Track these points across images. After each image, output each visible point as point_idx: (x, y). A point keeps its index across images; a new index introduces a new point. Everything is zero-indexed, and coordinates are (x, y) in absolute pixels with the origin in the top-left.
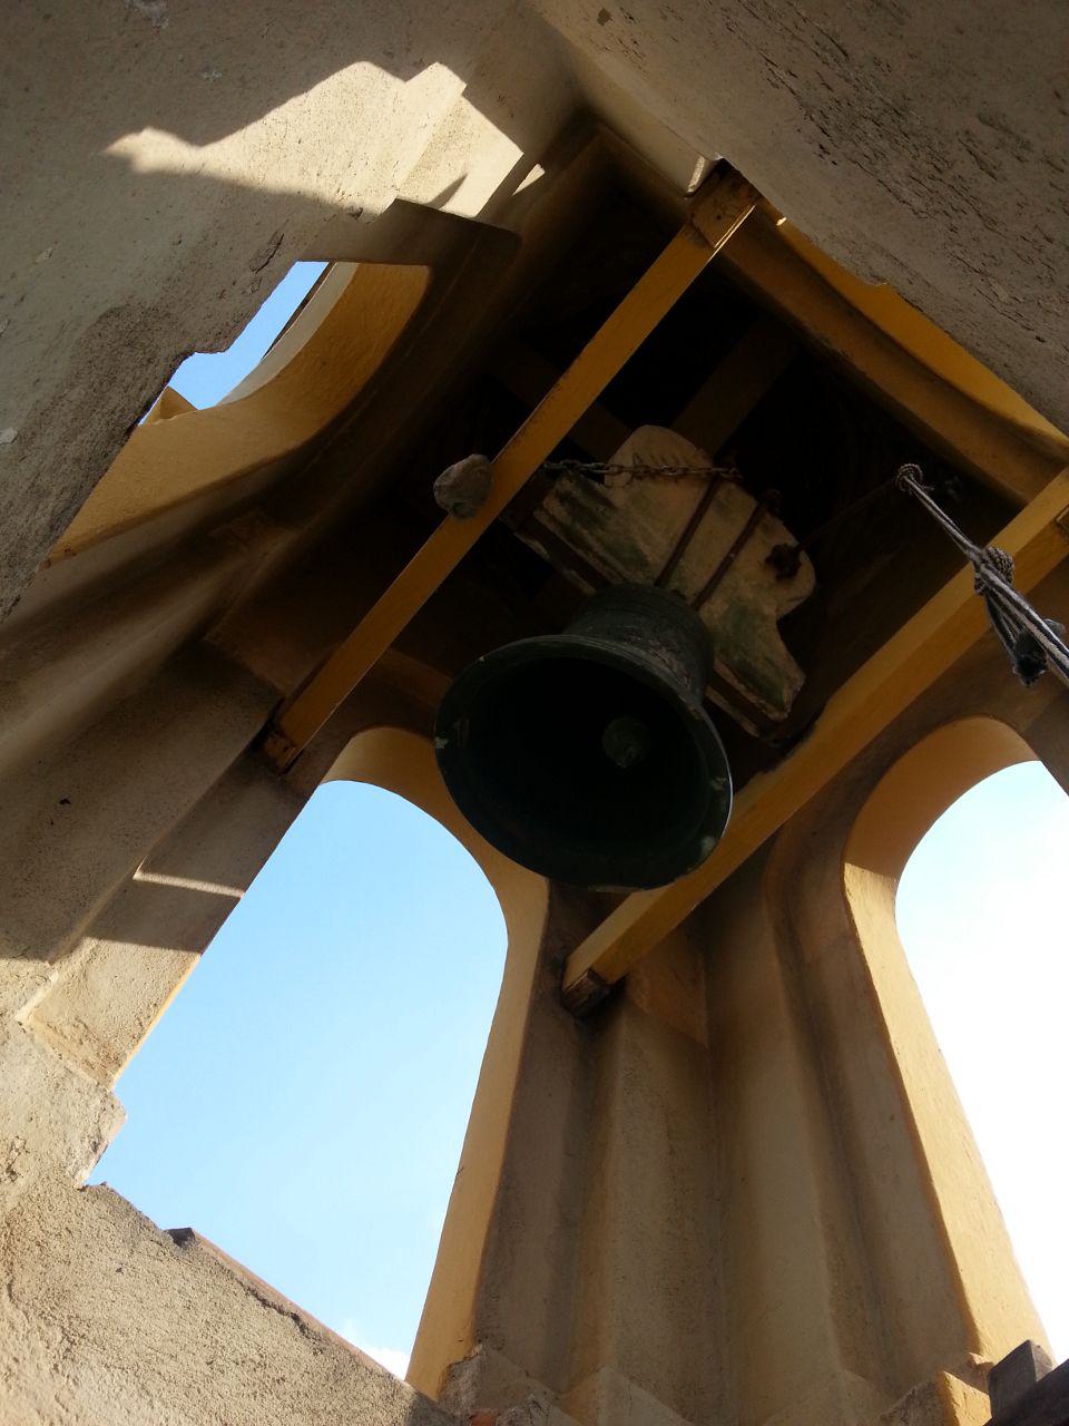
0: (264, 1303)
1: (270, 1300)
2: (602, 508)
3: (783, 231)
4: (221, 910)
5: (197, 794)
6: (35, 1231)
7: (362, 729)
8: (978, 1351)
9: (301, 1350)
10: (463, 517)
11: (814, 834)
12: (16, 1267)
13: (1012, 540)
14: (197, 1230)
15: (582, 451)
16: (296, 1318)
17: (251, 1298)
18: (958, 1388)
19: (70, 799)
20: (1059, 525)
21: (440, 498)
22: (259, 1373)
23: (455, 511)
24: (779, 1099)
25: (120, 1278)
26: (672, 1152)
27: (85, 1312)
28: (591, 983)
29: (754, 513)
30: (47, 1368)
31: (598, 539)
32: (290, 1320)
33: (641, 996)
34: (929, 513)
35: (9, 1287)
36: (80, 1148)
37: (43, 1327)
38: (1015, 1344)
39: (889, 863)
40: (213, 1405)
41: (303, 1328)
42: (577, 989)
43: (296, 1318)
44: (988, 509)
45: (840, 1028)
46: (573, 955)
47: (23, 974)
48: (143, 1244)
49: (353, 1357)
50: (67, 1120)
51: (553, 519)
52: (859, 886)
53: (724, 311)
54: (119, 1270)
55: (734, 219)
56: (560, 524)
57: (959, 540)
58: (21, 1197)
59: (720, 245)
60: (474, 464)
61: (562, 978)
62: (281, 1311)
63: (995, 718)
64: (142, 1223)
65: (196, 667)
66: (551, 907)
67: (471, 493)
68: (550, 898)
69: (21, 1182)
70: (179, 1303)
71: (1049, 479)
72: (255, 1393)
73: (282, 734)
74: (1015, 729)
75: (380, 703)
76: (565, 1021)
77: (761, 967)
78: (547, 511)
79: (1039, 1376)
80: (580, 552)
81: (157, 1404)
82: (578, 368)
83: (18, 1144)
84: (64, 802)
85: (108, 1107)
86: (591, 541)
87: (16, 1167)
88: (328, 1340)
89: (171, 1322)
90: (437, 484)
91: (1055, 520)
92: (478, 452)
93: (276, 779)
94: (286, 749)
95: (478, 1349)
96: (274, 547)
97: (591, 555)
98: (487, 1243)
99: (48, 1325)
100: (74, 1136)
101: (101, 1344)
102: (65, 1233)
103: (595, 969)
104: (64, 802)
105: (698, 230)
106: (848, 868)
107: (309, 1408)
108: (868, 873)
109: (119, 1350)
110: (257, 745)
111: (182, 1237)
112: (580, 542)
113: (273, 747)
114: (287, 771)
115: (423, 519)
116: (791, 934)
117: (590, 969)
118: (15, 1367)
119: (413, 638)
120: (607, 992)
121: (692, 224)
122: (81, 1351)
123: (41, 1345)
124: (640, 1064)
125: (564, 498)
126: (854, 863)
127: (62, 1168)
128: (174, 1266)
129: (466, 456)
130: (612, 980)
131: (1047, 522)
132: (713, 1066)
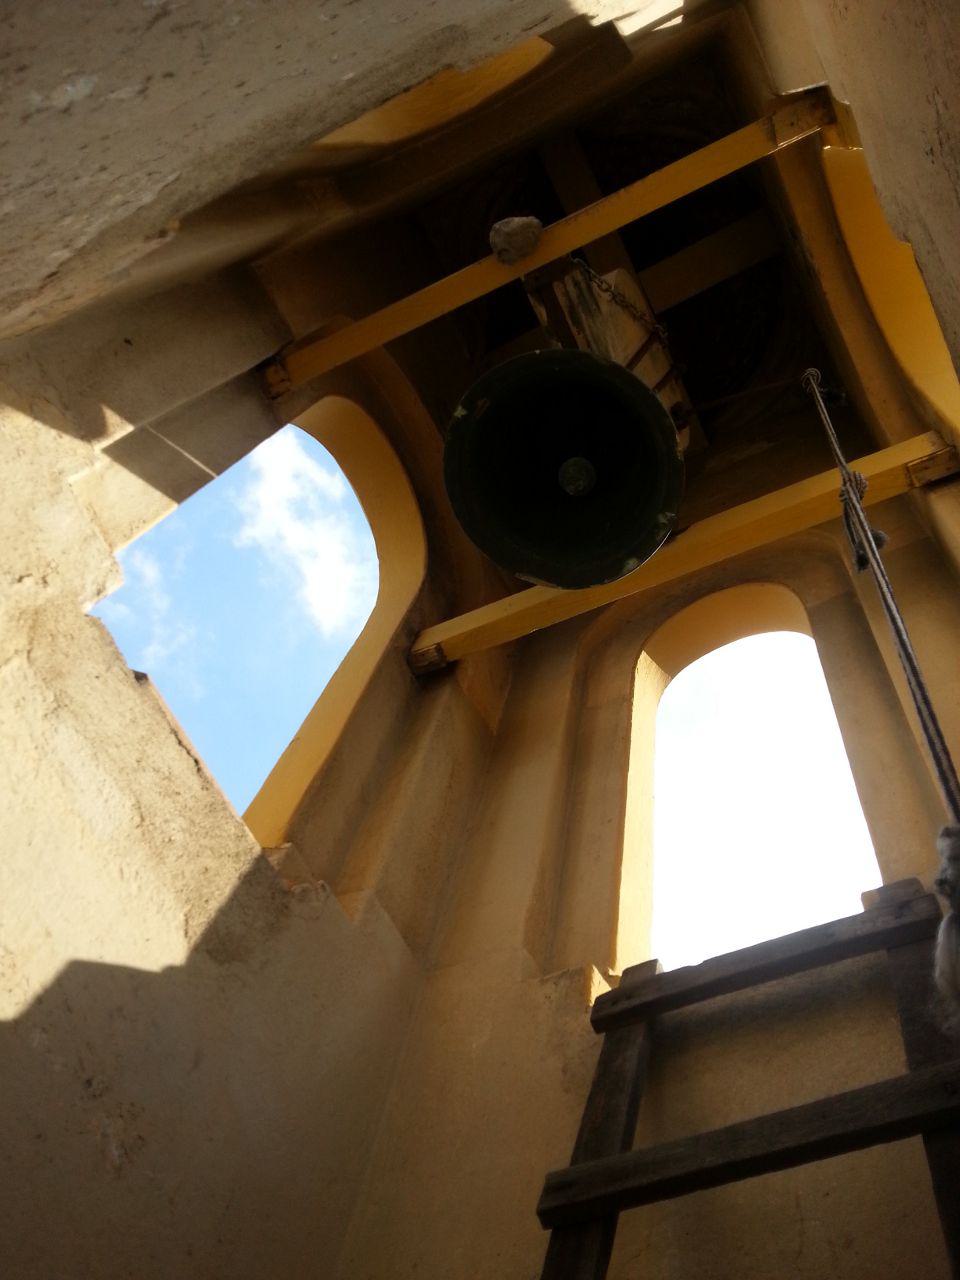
0: (180, 743)
1: (185, 742)
2: (594, 307)
3: (825, 155)
4: (202, 480)
5: (220, 381)
6: (51, 625)
7: (347, 395)
8: (613, 969)
9: (195, 782)
10: (503, 261)
11: (629, 622)
12: (35, 642)
13: (867, 467)
14: (150, 676)
15: (588, 258)
16: (196, 762)
17: (173, 736)
18: (597, 977)
19: (132, 342)
20: (907, 469)
21: (494, 238)
22: (166, 782)
23: (500, 253)
24: (533, 787)
25: (97, 683)
26: (450, 787)
27: (71, 691)
28: (436, 654)
29: (667, 374)
30: (40, 713)
31: (590, 326)
32: (192, 762)
33: (468, 675)
34: (822, 421)
35: (29, 652)
36: (91, 589)
37: (44, 687)
38: (652, 958)
39: (671, 665)
40: (135, 787)
41: (199, 770)
42: (423, 654)
43: (196, 762)
44: (863, 439)
45: (595, 756)
46: (428, 630)
47: (78, 451)
48: (116, 669)
49: (224, 803)
50: (87, 565)
51: (567, 294)
52: (645, 669)
53: (749, 194)
54: (97, 677)
55: (803, 131)
56: (570, 300)
57: (837, 454)
58: (48, 600)
59: (783, 144)
60: (525, 227)
61: (414, 642)
62: (188, 753)
63: (794, 591)
64: (117, 656)
65: (237, 288)
66: (421, 590)
67: (521, 245)
68: (423, 583)
69: (50, 590)
70: (129, 716)
71: (916, 434)
72: (160, 793)
73: (284, 367)
74: (804, 604)
75: (356, 382)
76: (406, 673)
77: (555, 696)
78: (565, 286)
79: (657, 973)
80: (574, 330)
81: (101, 768)
82: (639, 187)
83: (53, 565)
84: (128, 342)
85: (114, 570)
86: (586, 326)
87: (49, 579)
88: (212, 785)
89: (121, 725)
90: (497, 226)
91: (906, 464)
92: (537, 217)
93: (265, 401)
94: (283, 380)
95: (288, 845)
96: (336, 215)
97: (581, 336)
98: (311, 787)
99: (47, 688)
100: (90, 578)
101: (76, 716)
102: (69, 637)
103: (443, 645)
104: (128, 342)
105: (773, 126)
106: (644, 656)
107: (190, 818)
108: (654, 665)
109: (86, 726)
110: (261, 369)
111: (140, 677)
112: (578, 323)
113: (272, 374)
114: (274, 398)
115: (476, 249)
116: (584, 682)
117: (439, 644)
118: (22, 702)
119: (400, 346)
120: (444, 665)
121: (770, 119)
122: (63, 713)
123: (40, 698)
124: (446, 724)
125: (576, 284)
126: (653, 656)
127: (77, 595)
128: (131, 691)
129: (527, 216)
130: (451, 658)
131: (900, 464)
132: (496, 747)
